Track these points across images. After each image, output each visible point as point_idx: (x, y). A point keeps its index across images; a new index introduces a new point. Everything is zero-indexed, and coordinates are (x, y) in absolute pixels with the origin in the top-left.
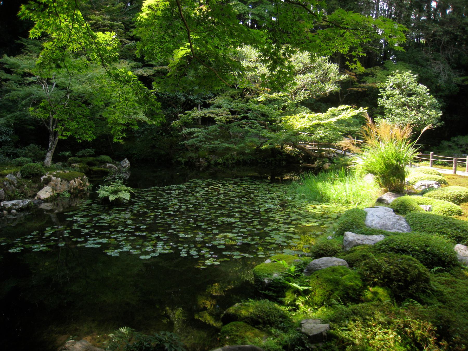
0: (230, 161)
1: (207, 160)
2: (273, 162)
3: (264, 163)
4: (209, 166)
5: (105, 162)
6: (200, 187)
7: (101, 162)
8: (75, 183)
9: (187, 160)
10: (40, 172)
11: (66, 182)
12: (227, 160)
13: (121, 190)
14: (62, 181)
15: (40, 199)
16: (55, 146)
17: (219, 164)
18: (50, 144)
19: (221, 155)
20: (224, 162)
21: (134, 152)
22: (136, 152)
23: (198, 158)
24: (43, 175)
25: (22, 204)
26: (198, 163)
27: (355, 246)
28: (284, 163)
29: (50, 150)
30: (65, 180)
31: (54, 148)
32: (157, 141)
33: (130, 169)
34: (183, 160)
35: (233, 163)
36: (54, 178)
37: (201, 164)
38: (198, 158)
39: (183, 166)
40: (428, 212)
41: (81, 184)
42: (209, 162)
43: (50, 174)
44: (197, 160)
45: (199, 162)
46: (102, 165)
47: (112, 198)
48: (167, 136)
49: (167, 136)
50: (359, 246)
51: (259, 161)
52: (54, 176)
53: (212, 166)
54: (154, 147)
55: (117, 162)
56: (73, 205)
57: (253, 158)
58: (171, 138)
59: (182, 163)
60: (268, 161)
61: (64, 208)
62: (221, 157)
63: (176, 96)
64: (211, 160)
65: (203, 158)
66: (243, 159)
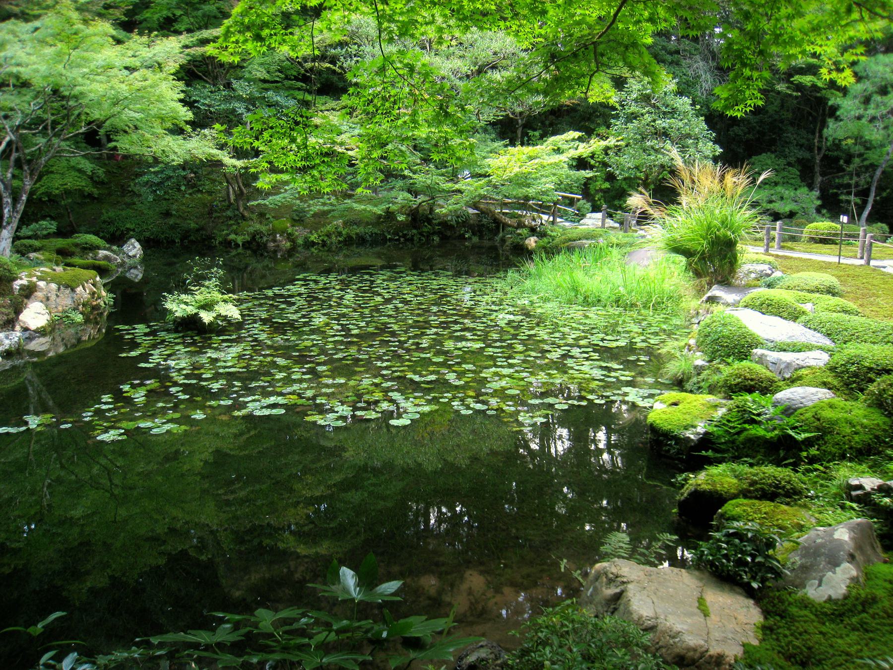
0: (334, 238)
1: (290, 237)
2: (415, 238)
3: (398, 240)
4: (291, 252)
5: (94, 248)
6: (334, 288)
7: (85, 249)
8: (83, 293)
9: (248, 238)
10: (9, 271)
11: (68, 291)
12: (329, 235)
13: (218, 302)
14: (59, 289)
15: (26, 329)
16: (19, 216)
17: (313, 244)
18: (6, 211)
19: (315, 227)
20: (323, 241)
21: (128, 226)
22: (132, 227)
23: (273, 233)
24: (15, 279)
25: (7, 342)
26: (272, 244)
27: (796, 370)
28: (436, 238)
29: (8, 223)
30: (67, 286)
31: (17, 220)
32: (171, 201)
33: (145, 260)
34: (240, 240)
35: (340, 242)
36: (42, 284)
37: (278, 246)
38: (273, 233)
39: (240, 250)
40: (78, 348)
41: (94, 293)
42: (293, 241)
43: (30, 276)
44: (271, 238)
45: (274, 241)
46: (87, 254)
47: (207, 317)
48: (190, 191)
49: (190, 191)
50: (803, 370)
51: (389, 237)
52: (40, 279)
53: (299, 249)
54: (167, 214)
55: (115, 248)
56: (84, 338)
57: (376, 231)
58: (199, 195)
59: (237, 245)
60: (404, 236)
61: (66, 345)
62: (316, 231)
63: (234, 110)
64: (297, 237)
65: (282, 233)
66: (357, 234)
